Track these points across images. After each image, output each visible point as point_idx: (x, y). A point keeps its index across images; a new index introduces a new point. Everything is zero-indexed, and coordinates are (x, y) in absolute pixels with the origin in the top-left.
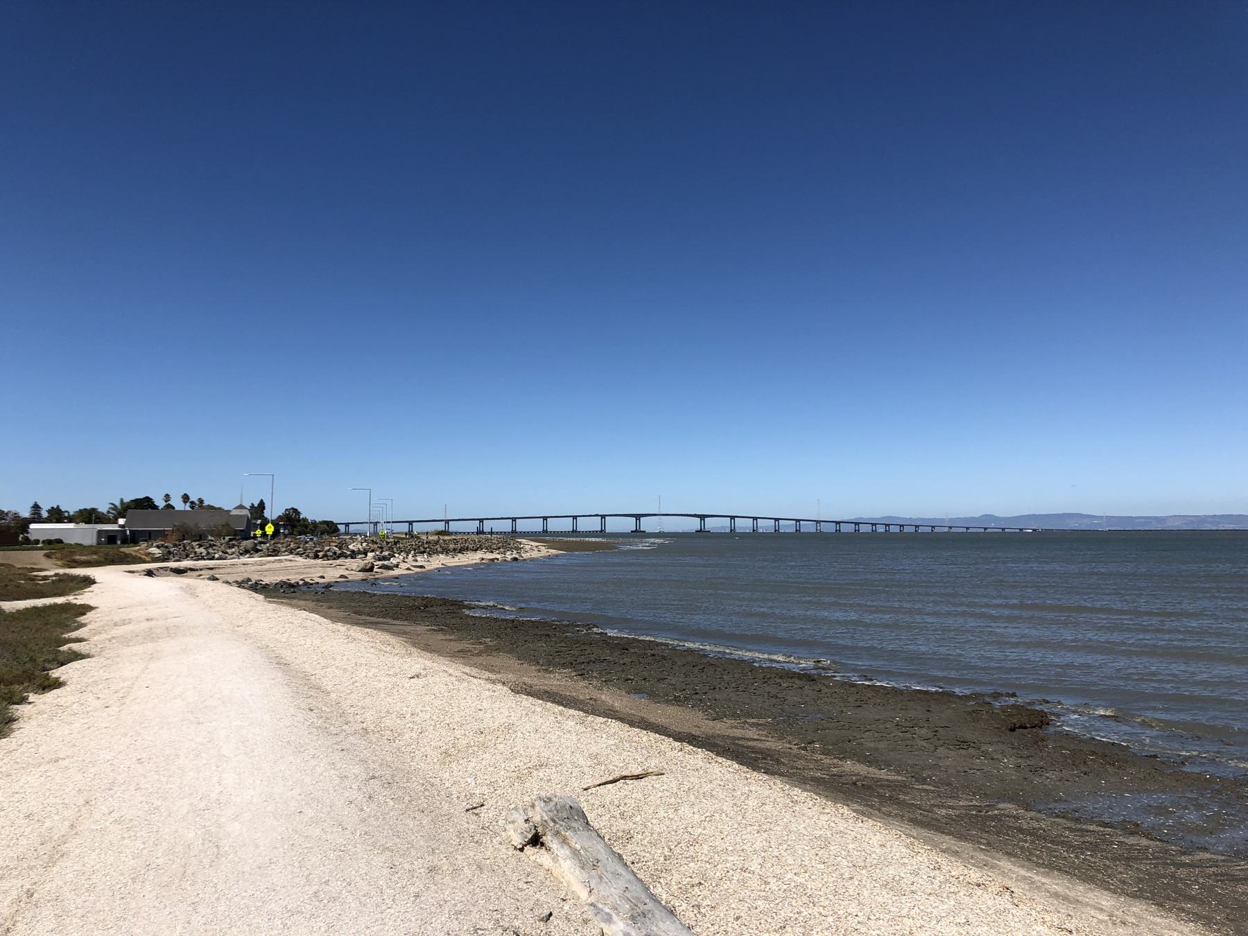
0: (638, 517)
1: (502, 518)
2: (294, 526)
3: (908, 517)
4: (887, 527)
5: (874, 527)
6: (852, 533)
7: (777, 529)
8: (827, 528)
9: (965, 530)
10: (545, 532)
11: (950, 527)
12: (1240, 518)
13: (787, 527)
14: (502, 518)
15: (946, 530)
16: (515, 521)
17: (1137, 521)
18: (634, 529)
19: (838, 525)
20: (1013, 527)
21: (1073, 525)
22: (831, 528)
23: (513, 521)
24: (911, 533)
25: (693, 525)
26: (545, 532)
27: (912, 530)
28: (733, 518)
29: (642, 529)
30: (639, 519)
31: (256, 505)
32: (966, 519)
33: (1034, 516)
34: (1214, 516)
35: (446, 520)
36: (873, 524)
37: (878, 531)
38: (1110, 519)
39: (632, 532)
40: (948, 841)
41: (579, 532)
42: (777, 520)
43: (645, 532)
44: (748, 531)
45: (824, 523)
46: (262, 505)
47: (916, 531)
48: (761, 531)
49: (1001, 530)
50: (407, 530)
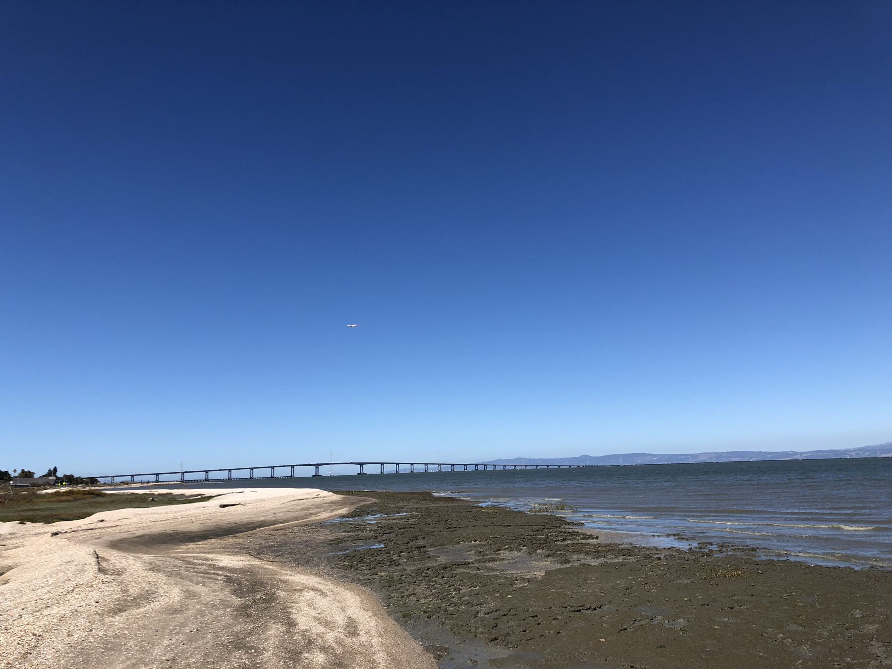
1: (284, 466)
2: (71, 482)
3: (532, 458)
8: (445, 469)
9: (546, 467)
10: (207, 480)
13: (446, 469)
17: (680, 457)
18: (315, 474)
20: (575, 464)
21: (640, 461)
22: (448, 469)
25: (355, 470)
26: (207, 480)
27: (501, 468)
28: (412, 464)
29: (320, 474)
30: (318, 467)
31: (52, 470)
34: (752, 452)
37: (479, 470)
38: (719, 455)
40: (193, 534)
43: (321, 476)
44: (422, 472)
45: (161, 475)
46: (55, 470)
49: (569, 467)
50: (204, 478)
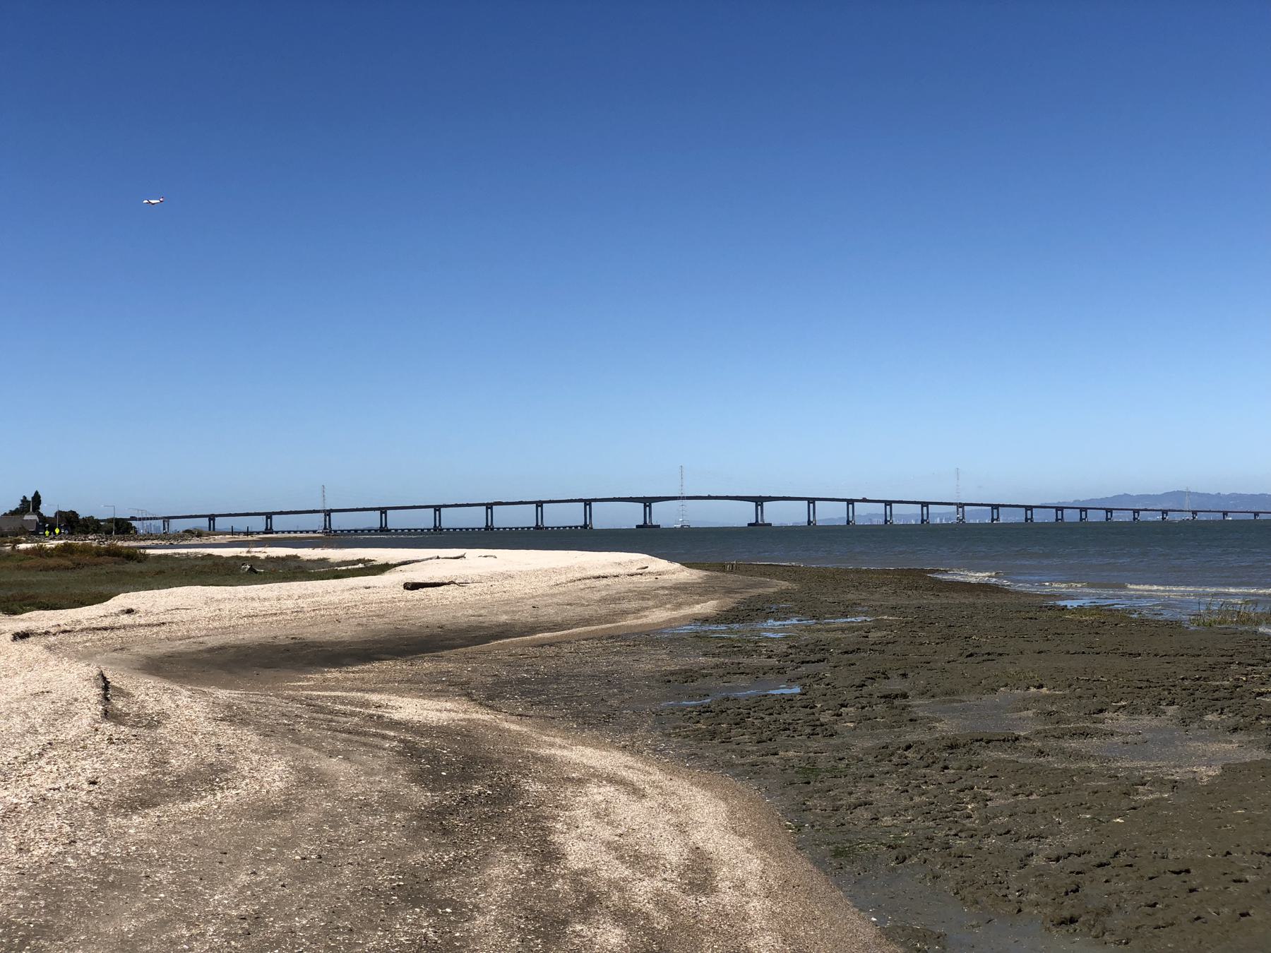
0: (759, 501)
1: (709, 498)
2: (73, 527)
3: (1213, 492)
4: (1084, 513)
5: (1029, 512)
6: (1130, 522)
7: (925, 518)
9: (1251, 517)
11: (1194, 513)
12: (1262, 498)
14: (709, 498)
15: (1189, 516)
16: (439, 510)
19: (995, 511)
23: (487, 509)
24: (804, 526)
26: (383, 529)
32: (1253, 497)
33: (1149, 496)
35: (324, 511)
36: (1082, 510)
39: (638, 526)
41: (547, 528)
42: (925, 504)
43: (770, 525)
47: (1134, 519)
48: (938, 521)
50: (376, 524)
